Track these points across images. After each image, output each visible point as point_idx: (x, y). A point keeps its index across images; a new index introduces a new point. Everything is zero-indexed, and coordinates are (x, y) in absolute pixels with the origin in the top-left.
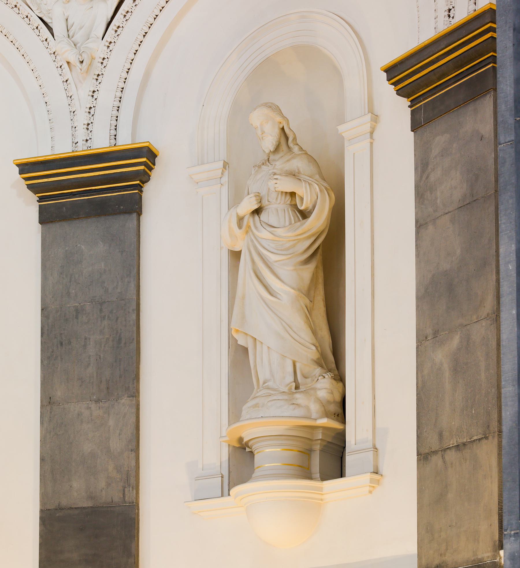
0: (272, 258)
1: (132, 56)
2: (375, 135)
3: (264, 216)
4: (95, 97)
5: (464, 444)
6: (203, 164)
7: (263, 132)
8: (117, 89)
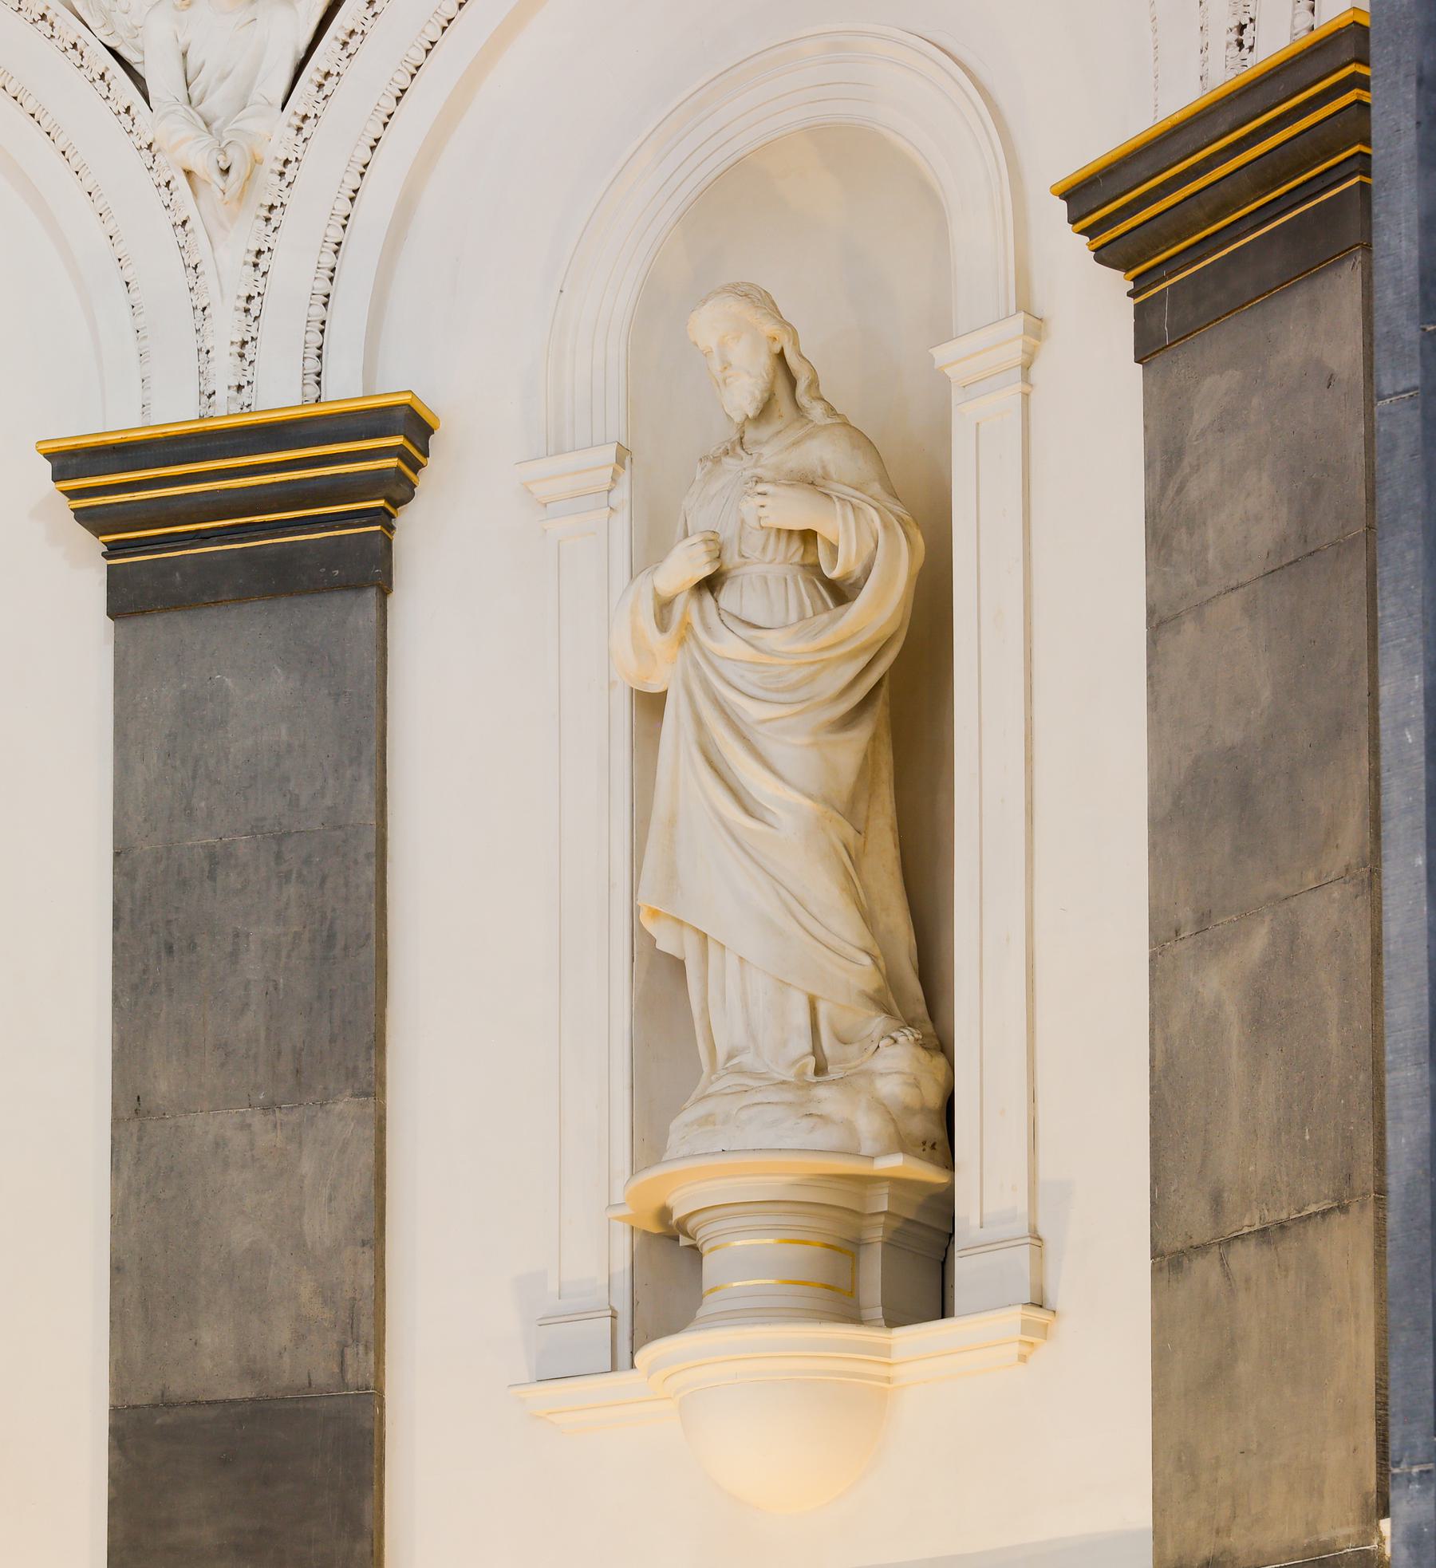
0: (752, 711)
1: (364, 155)
2: (1036, 373)
3: (728, 596)
4: (263, 268)
5: (1282, 1227)
6: (560, 451)
7: (726, 365)
8: (323, 246)
